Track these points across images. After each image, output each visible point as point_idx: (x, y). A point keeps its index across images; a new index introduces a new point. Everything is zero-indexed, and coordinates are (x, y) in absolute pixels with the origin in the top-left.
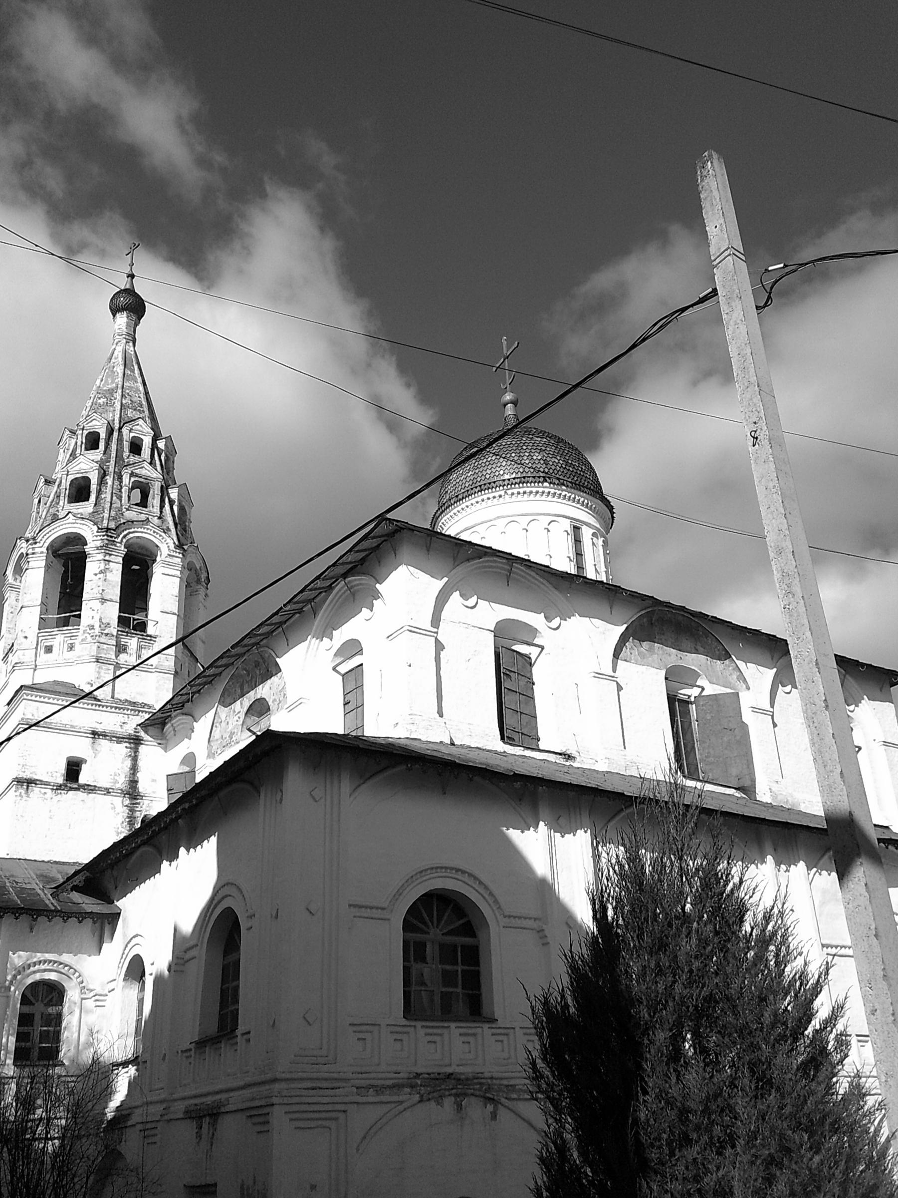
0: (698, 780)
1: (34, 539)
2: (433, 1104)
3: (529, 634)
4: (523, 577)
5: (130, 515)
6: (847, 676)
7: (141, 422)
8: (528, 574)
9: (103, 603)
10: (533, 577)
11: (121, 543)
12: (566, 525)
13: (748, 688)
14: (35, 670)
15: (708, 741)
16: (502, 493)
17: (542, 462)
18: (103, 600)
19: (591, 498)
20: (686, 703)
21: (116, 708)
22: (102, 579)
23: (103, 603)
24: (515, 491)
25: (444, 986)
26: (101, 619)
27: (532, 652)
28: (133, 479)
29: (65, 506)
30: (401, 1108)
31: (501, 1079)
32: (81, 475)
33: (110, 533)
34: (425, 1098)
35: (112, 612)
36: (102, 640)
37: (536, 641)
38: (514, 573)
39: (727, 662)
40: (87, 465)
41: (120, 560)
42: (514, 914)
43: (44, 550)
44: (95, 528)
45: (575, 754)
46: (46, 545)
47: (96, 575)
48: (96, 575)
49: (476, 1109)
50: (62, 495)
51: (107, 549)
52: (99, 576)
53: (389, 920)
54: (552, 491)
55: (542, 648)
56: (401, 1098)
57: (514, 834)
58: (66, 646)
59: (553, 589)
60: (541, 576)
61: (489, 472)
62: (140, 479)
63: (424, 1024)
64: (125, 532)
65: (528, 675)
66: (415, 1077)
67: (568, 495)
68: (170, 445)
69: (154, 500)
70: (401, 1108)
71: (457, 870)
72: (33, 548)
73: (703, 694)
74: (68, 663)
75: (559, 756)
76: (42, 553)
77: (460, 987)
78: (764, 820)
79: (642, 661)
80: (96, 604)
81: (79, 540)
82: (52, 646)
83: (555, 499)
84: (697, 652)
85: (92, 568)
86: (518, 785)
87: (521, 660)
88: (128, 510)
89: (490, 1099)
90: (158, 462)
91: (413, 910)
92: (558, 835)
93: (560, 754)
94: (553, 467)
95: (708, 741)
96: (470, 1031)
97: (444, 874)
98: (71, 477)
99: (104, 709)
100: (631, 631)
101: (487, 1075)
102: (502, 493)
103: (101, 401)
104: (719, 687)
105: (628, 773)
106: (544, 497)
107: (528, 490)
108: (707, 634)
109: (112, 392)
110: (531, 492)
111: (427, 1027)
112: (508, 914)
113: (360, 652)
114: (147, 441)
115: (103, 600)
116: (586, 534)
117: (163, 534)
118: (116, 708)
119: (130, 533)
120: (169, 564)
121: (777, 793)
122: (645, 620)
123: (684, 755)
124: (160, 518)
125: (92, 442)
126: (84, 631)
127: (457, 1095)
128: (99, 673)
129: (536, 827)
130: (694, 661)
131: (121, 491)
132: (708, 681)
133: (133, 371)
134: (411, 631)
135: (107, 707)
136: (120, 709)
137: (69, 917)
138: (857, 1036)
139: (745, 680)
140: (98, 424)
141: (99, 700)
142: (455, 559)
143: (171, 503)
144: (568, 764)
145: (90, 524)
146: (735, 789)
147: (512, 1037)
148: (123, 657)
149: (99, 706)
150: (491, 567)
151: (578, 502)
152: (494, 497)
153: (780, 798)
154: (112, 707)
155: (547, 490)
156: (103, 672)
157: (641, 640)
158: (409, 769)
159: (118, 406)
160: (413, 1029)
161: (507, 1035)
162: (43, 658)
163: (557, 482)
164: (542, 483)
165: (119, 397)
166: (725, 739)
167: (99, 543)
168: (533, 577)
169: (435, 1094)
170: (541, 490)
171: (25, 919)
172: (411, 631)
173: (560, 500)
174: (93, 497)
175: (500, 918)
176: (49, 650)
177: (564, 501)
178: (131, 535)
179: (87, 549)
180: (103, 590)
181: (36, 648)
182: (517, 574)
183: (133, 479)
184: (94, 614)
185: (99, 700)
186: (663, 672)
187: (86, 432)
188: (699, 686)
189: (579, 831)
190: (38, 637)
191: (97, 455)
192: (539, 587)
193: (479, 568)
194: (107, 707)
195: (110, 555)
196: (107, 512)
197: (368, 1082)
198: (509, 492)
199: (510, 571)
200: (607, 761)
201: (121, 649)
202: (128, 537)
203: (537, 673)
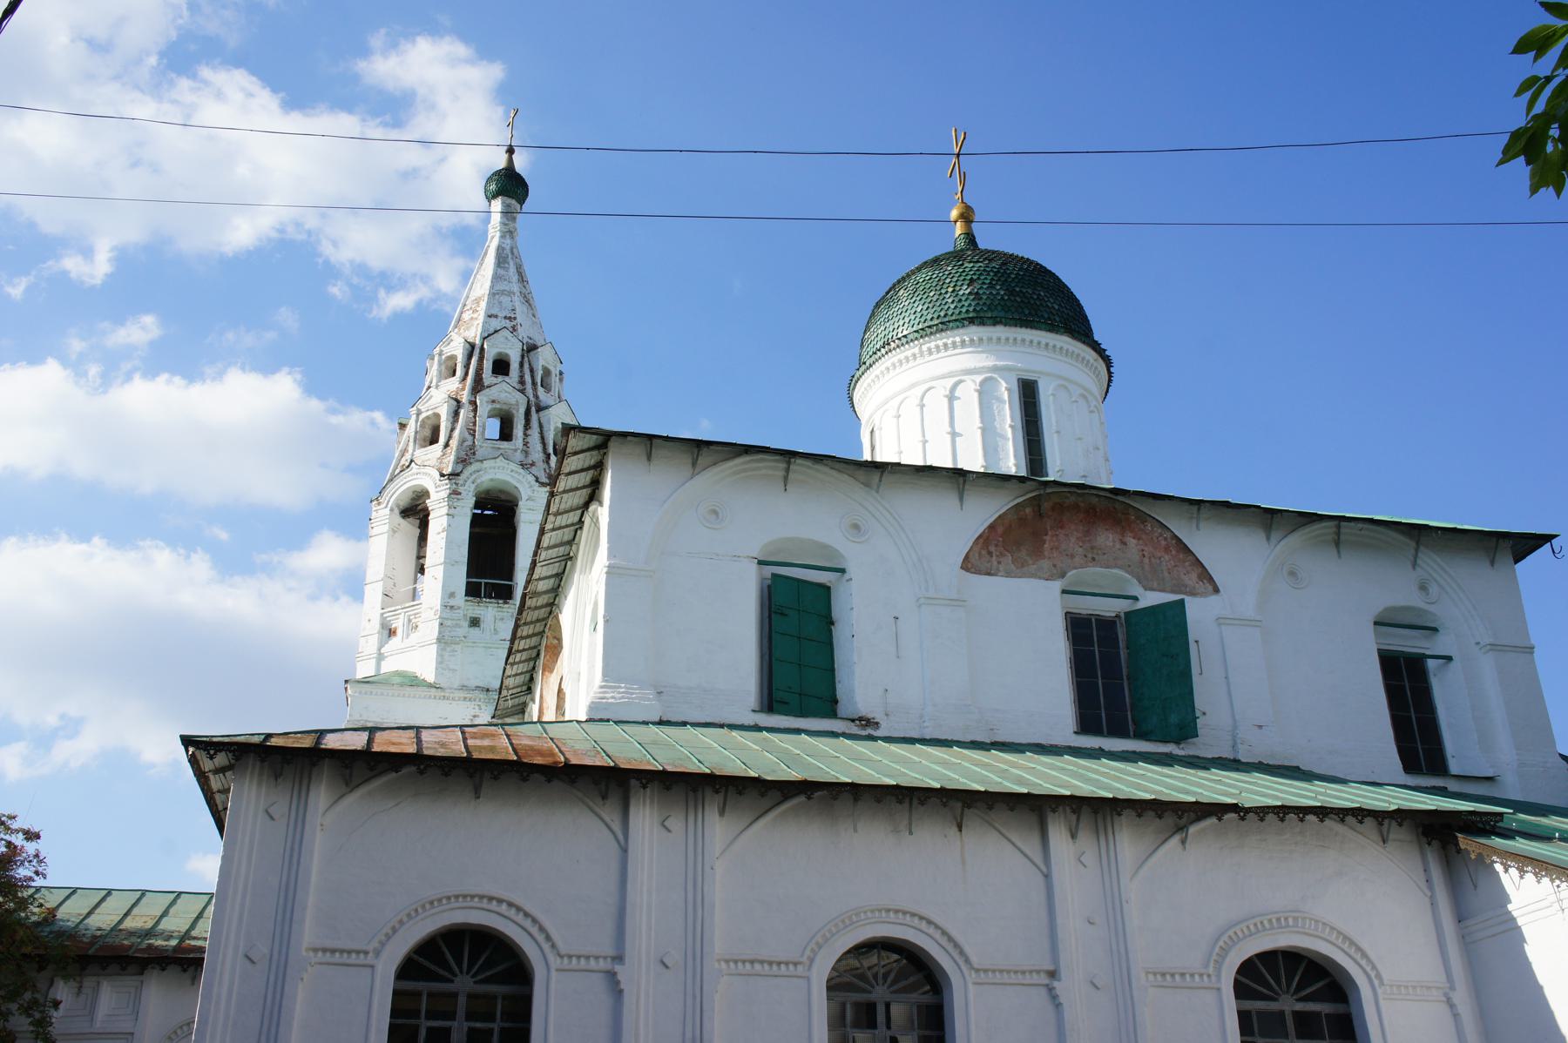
16: (916, 350)
43: (387, 511)
45: (878, 716)
69: (518, 430)
77: (491, 1025)
78: (984, 430)
91: (1268, 957)
102: (916, 350)
113: (1300, 1036)
122: (1028, 510)
137: (1285, 814)
139: (1211, 580)
146: (654, 723)
152: (900, 362)
158: (421, 772)
171: (173, 971)
175: (551, 957)
191: (453, 384)
193: (735, 473)
199: (1338, 534)
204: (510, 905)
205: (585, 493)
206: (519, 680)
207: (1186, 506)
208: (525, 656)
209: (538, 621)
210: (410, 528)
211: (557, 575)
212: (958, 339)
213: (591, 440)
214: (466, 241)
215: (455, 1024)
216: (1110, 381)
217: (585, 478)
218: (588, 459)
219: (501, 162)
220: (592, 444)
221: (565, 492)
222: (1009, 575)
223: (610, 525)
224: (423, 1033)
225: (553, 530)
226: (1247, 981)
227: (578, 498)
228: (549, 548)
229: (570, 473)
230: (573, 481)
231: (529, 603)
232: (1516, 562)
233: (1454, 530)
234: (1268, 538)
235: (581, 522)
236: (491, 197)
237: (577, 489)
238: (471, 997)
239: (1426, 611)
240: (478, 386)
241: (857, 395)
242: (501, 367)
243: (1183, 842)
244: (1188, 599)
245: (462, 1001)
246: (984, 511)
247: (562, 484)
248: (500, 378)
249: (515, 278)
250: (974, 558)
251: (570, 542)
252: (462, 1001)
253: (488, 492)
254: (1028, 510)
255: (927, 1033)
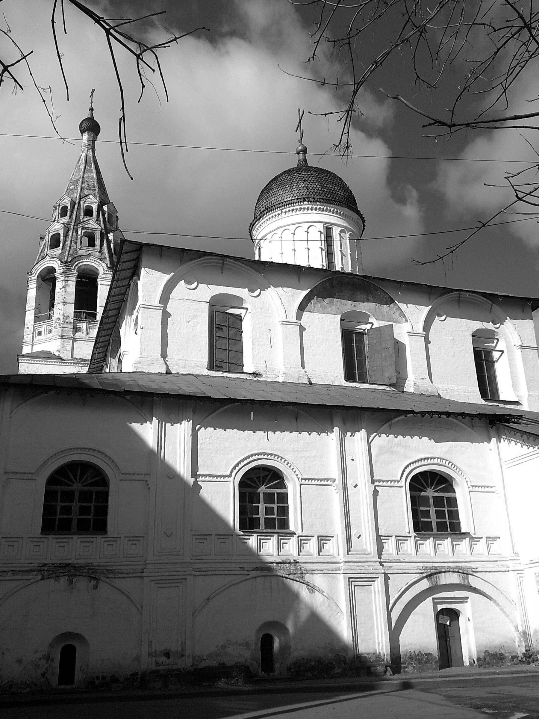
0: (367, 383)
1: (31, 272)
2: (52, 581)
3: (238, 302)
4: (235, 267)
5: (80, 252)
6: (494, 305)
7: (91, 196)
8: (236, 264)
9: (64, 305)
10: (240, 265)
11: (74, 269)
12: (321, 227)
13: (407, 321)
14: (33, 346)
15: (373, 357)
16: (280, 212)
17: (305, 188)
18: (65, 303)
19: (339, 207)
20: (361, 334)
21: (74, 363)
22: (66, 290)
23: (64, 305)
24: (287, 210)
25: (80, 515)
26: (63, 314)
27: (242, 312)
28: (83, 231)
29: (48, 251)
30: (29, 583)
31: (107, 566)
32: (55, 232)
33: (67, 264)
34: (45, 577)
35: (71, 309)
36: (64, 326)
37: (244, 306)
38: (226, 264)
39: (392, 305)
40: (58, 227)
41: (74, 279)
42: (130, 472)
43: (36, 278)
44: (59, 262)
45: (261, 371)
46: (37, 275)
47: (61, 289)
48: (61, 289)
49: (82, 583)
50: (47, 245)
51: (65, 274)
52: (63, 289)
53: (35, 480)
54: (310, 206)
55: (247, 309)
56: (29, 577)
57: (136, 426)
58: (48, 330)
59: (255, 272)
60: (246, 265)
61: (273, 199)
62: (88, 231)
63: (55, 536)
64: (77, 263)
65: (238, 327)
66: (43, 566)
67: (322, 207)
68: (112, 208)
69: (97, 243)
70: (29, 583)
71: (90, 449)
72: (31, 278)
73: (373, 327)
74: (48, 340)
75: (248, 375)
76: (34, 279)
79: (324, 310)
80: (61, 306)
81: (53, 270)
82: (41, 332)
83: (313, 211)
84: (368, 301)
85: (59, 285)
86: (128, 397)
87: (231, 319)
88: (80, 249)
89: (92, 577)
90: (101, 219)
92: (168, 425)
93: (250, 374)
94: (312, 191)
95: (373, 357)
96: (88, 540)
97: (79, 452)
98: (51, 234)
99: (67, 364)
100: (315, 292)
101: (95, 564)
102: (280, 212)
103: (71, 187)
104: (384, 322)
105: (300, 381)
106: (305, 211)
107: (294, 208)
108: (377, 289)
109: (77, 180)
110: (297, 209)
111: (57, 538)
112: (123, 472)
114: (95, 207)
115: (65, 303)
116: (336, 232)
117: (100, 261)
118: (74, 363)
119: (79, 263)
120: (103, 278)
121: (420, 386)
122: (327, 284)
123: (353, 368)
124: (100, 252)
125: (64, 212)
126: (56, 322)
127: (69, 575)
128: (63, 344)
129: (151, 421)
130: (364, 307)
131: (77, 239)
132: (374, 318)
133: (91, 167)
134: (144, 308)
135: (69, 363)
136: (77, 363)
138: (396, 536)
140: (67, 201)
141: (63, 360)
142: (181, 260)
143: (109, 242)
144: (255, 379)
145: (57, 260)
147: (118, 542)
148: (78, 335)
149: (64, 363)
150: (210, 263)
151: (330, 212)
153: (421, 388)
154: (71, 363)
155: (306, 206)
156: (65, 344)
157: (324, 298)
158: (58, 394)
159: (79, 189)
160: (47, 539)
161: (139, 540)
162: (38, 338)
163: (312, 200)
164: (303, 202)
165: (80, 184)
166: (383, 355)
167: (62, 271)
168: (240, 265)
169: (54, 575)
170: (302, 207)
172: (144, 308)
173: (316, 212)
174: (61, 245)
176: (40, 334)
177: (320, 212)
178: (81, 264)
179: (56, 274)
180: (64, 298)
181: (33, 333)
182: (229, 265)
183: (83, 231)
184: (60, 311)
185: (63, 360)
186: (339, 317)
187: (61, 207)
188: (370, 323)
189: (184, 421)
190: (34, 327)
191: (65, 220)
192: (245, 271)
194: (69, 363)
195: (68, 277)
196: (67, 252)
197: (10, 569)
198: (284, 211)
200: (284, 375)
201: (76, 330)
202: (79, 265)
203: (246, 326)
204: (99, 452)
205: (131, 271)
206: (101, 355)
207: (395, 284)
208: (103, 344)
209: (109, 329)
210: (47, 287)
211: (118, 308)
212: (332, 209)
213: (135, 247)
214: (183, 357)
215: (74, 504)
216: (364, 229)
217: (132, 264)
218: (134, 256)
219: (87, 115)
220: (134, 249)
221: (121, 270)
222: (318, 312)
223: (84, 518)
224: (444, 509)
225: (116, 288)
226: (413, 483)
227: (128, 273)
228: (113, 296)
229: (125, 262)
230: (125, 266)
231: (105, 320)
232: (533, 311)
233: (508, 296)
234: (430, 299)
235: (129, 285)
236: (82, 131)
237: (128, 269)
238: (81, 493)
239: (494, 331)
240: (78, 222)
241: (254, 233)
242: (88, 212)
243: (390, 426)
244: (394, 324)
245: (77, 495)
246: (315, 282)
247: (120, 267)
248: (88, 218)
249: (94, 171)
250: (220, 355)
251: (124, 294)
252: (77, 495)
253: (84, 270)
254: (327, 284)
255: (286, 505)
